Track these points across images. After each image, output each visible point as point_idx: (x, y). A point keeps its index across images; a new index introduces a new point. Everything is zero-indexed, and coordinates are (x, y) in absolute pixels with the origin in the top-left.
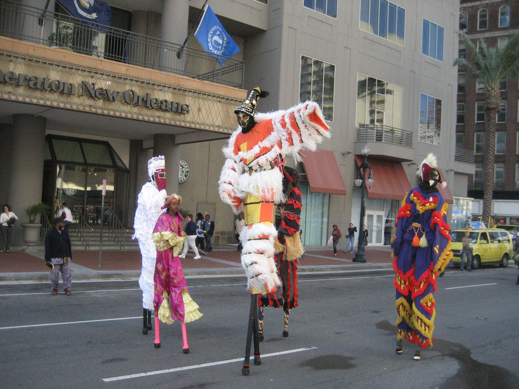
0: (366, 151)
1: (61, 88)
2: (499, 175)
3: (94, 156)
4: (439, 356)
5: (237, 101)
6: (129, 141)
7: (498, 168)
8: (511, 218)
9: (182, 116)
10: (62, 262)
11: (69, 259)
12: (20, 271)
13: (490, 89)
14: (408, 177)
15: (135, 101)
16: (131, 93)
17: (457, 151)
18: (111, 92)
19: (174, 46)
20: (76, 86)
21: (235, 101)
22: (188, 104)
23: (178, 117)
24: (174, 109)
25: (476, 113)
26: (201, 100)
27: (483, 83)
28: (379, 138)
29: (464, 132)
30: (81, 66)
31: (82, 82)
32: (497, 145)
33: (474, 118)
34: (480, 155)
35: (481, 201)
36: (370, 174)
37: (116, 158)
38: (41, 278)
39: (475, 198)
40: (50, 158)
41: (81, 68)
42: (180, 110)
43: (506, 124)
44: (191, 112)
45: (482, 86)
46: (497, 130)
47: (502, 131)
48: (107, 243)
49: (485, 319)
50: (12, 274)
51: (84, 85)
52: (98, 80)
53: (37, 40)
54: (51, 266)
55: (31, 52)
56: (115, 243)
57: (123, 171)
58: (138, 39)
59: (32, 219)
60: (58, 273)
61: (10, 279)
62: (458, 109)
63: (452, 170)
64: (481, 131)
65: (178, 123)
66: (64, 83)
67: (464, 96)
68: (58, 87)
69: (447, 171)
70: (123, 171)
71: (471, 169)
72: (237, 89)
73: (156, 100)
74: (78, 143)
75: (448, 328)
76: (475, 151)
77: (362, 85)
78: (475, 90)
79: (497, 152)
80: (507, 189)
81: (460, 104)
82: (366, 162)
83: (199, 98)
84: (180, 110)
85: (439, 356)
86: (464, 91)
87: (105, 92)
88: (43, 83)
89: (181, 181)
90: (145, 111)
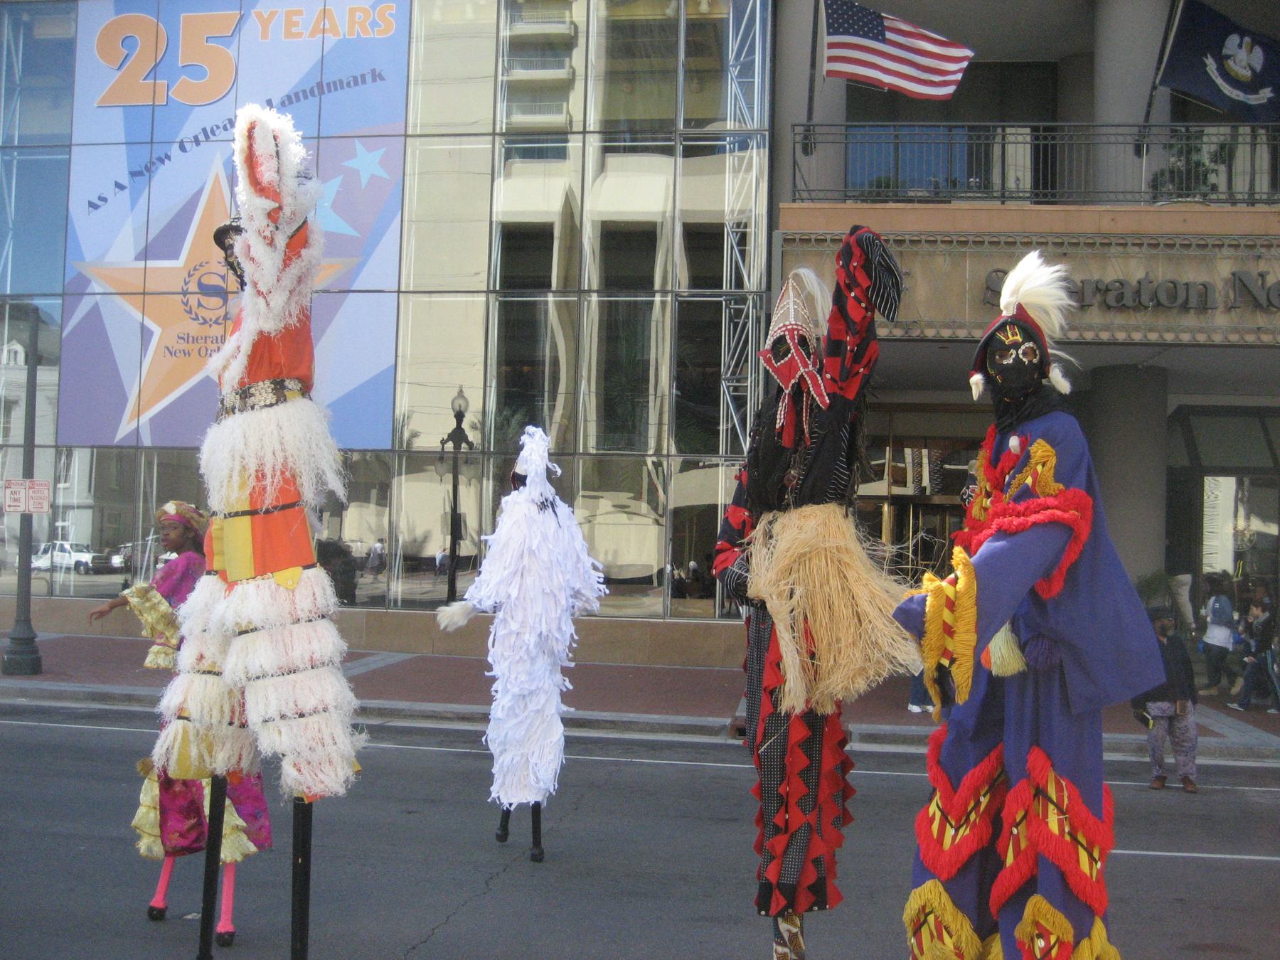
1: (1180, 300)
10: (1170, 713)
11: (1189, 704)
19: (1120, 130)
20: (1220, 285)
30: (999, 234)
31: (1234, 274)
41: (1227, 242)
53: (1129, 196)
54: (1145, 721)
55: (1106, 225)
58: (1062, 138)
60: (511, 712)
66: (1187, 284)
68: (1173, 296)
88: (1138, 293)
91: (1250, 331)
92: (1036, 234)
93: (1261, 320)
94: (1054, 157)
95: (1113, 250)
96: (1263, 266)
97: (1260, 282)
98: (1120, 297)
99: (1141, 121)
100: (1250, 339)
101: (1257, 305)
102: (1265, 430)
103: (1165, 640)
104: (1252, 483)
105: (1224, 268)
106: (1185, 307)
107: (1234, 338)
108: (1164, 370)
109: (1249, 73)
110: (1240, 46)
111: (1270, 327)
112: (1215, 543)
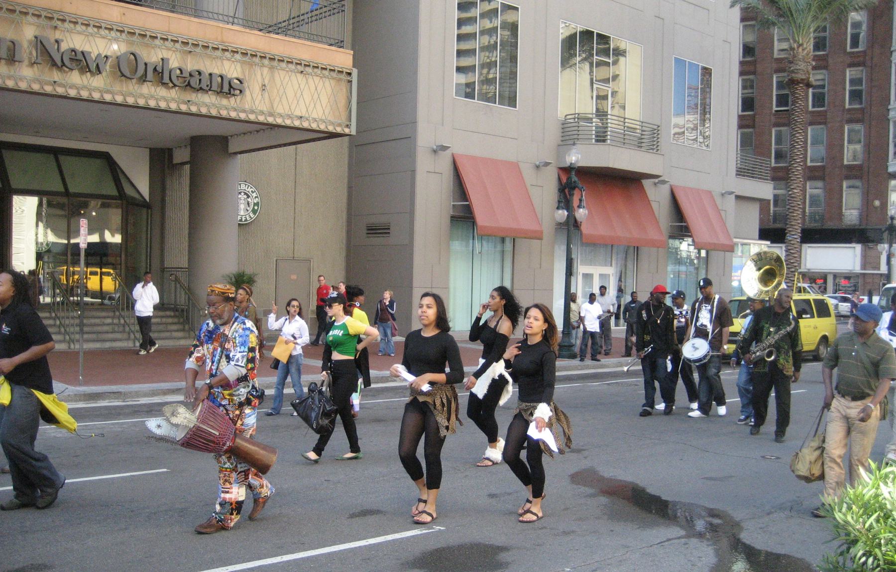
0: (574, 158)
2: (814, 201)
3: (83, 178)
4: (679, 538)
5: (334, 70)
6: (147, 152)
7: (814, 189)
8: (835, 276)
9: (232, 100)
13: (795, 46)
14: (655, 206)
15: (141, 71)
16: (132, 57)
17: (743, 159)
18: (93, 56)
20: (25, 45)
21: (331, 70)
22: (241, 77)
23: (225, 102)
24: (215, 87)
25: (775, 93)
26: (266, 70)
27: (787, 40)
28: (601, 138)
29: (753, 127)
30: (30, 7)
31: (36, 37)
32: (811, 147)
33: (772, 104)
34: (782, 167)
35: (783, 246)
36: (581, 200)
37: (123, 180)
39: (772, 242)
41: (31, 11)
42: (226, 88)
43: (826, 111)
44: (247, 93)
45: (785, 45)
46: (811, 124)
47: (820, 123)
48: (111, 336)
49: (778, 458)
51: (40, 44)
52: (67, 34)
56: (125, 336)
57: (137, 205)
62: (744, 88)
63: (732, 193)
64: (784, 125)
65: (224, 113)
66: (210, 75)
67: (754, 63)
69: (723, 195)
70: (137, 205)
71: (765, 190)
72: (333, 48)
73: (180, 69)
74: (52, 157)
75: (707, 478)
76: (773, 161)
77: (569, 43)
78: (773, 53)
79: (812, 161)
80: (831, 225)
81: (745, 77)
82: (574, 178)
83: (263, 66)
84: (226, 88)
85: (679, 538)
86: (753, 55)
87: (80, 57)
89: (246, 220)
90: (162, 92)
91: (48, 83)
93: (56, 76)
96: (58, 35)
97: (56, 47)
100: (48, 89)
101: (54, 64)
102: (57, 160)
104: (49, 204)
105: (28, 32)
106: (143, 79)
107: (36, 87)
111: (63, 82)
112: (22, 246)
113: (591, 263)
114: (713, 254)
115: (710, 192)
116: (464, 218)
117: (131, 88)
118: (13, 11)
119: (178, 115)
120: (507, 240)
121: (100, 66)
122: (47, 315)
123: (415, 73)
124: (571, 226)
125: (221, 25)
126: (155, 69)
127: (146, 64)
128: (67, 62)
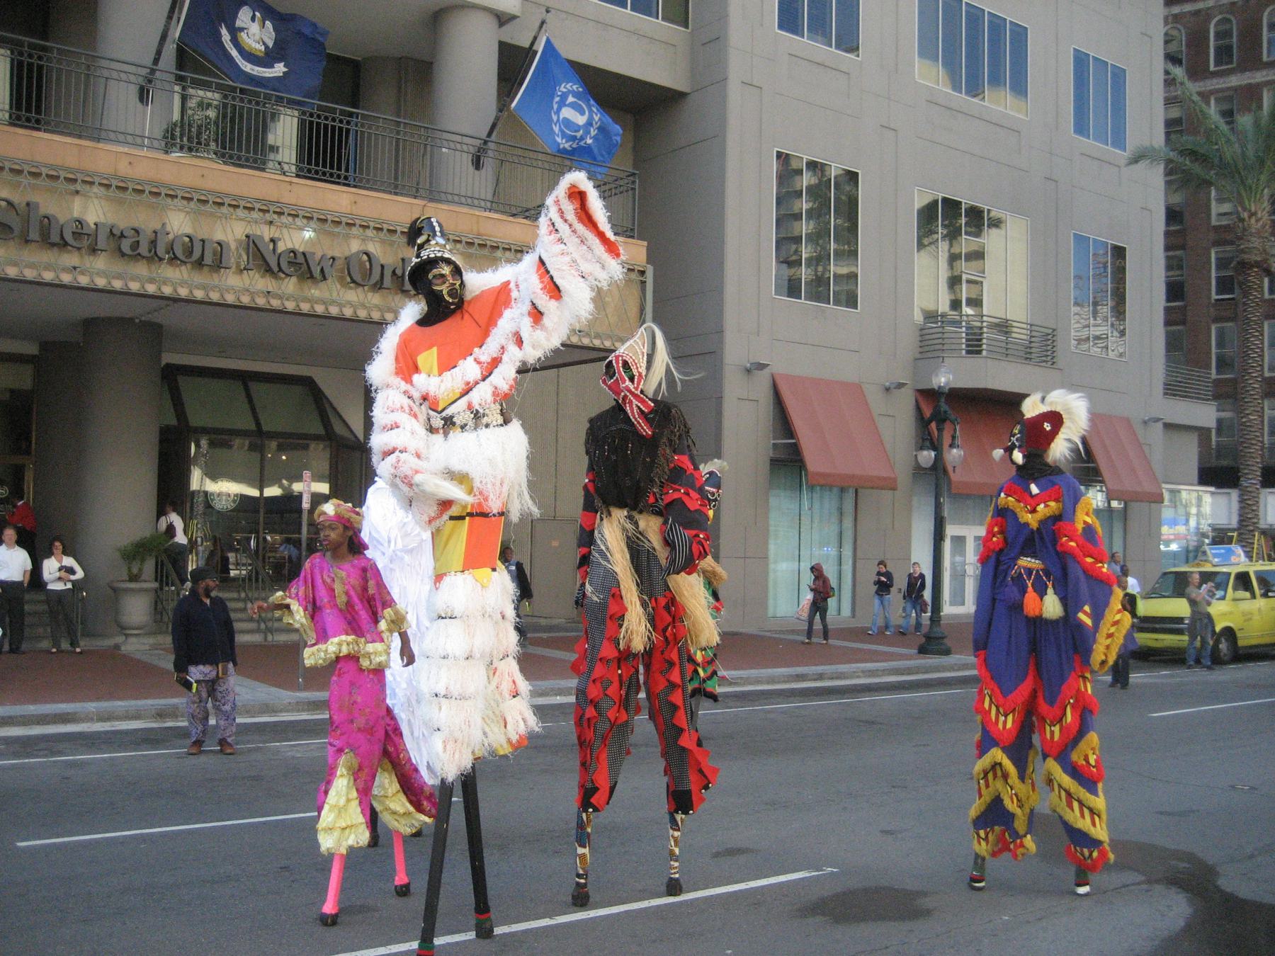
0: (943, 380)
1: (197, 254)
11: (231, 665)
12: (111, 697)
13: (1246, 215)
16: (365, 257)
17: (1169, 371)
19: (466, 140)
20: (233, 246)
25: (1213, 274)
28: (974, 348)
29: (1184, 323)
31: (247, 236)
35: (1234, 494)
36: (953, 437)
38: (161, 715)
40: (173, 421)
45: (1227, 207)
49: (1252, 788)
50: (91, 706)
52: (285, 231)
53: (135, 140)
55: (123, 169)
58: (370, 128)
59: (135, 571)
61: (88, 718)
62: (1169, 268)
63: (1158, 420)
69: (1145, 422)
71: (1205, 414)
76: (1214, 371)
81: (1171, 253)
82: (944, 407)
87: (301, 259)
88: (153, 243)
91: (65, 270)
92: (46, 166)
94: (362, 140)
95: (95, 189)
97: (271, 246)
98: (136, 245)
99: (484, 135)
101: (268, 270)
103: (208, 601)
108: (160, 326)
109: (263, 48)
110: (253, 19)
113: (963, 522)
114: (1134, 506)
115: (1128, 420)
116: (788, 462)
117: (362, 296)
118: (158, 194)
119: (355, 324)
120: (851, 491)
121: (326, 271)
122: (235, 595)
123: (721, 264)
124: (938, 470)
125: (477, 213)
126: (394, 272)
127: (382, 266)
128: (284, 266)
